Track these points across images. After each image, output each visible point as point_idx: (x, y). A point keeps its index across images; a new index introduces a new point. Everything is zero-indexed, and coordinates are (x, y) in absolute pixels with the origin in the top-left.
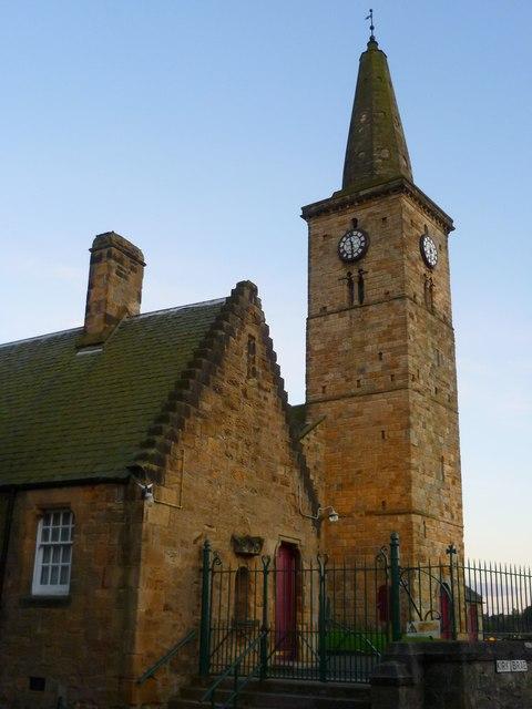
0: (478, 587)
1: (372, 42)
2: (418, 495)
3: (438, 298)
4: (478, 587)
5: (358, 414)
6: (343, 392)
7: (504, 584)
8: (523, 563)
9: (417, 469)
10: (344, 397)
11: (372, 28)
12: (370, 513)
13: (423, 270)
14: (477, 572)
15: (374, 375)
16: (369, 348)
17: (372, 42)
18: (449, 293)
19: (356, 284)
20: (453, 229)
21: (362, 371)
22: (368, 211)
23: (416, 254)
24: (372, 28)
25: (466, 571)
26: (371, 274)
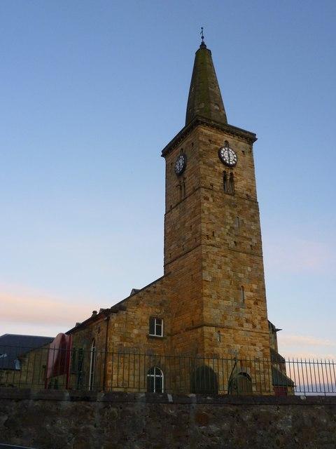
0: (297, 379)
1: (203, 45)
2: (211, 313)
3: (240, 186)
4: (297, 379)
5: (183, 267)
6: (178, 254)
7: (305, 376)
8: (332, 357)
9: (210, 296)
10: (177, 258)
11: (203, 38)
12: (187, 329)
13: (222, 168)
14: (331, 365)
15: (189, 240)
16: (187, 224)
17: (203, 45)
18: (253, 180)
19: (181, 187)
20: (256, 139)
21: (184, 240)
22: (186, 142)
23: (215, 159)
24: (203, 38)
25: (287, 364)
26: (187, 179)
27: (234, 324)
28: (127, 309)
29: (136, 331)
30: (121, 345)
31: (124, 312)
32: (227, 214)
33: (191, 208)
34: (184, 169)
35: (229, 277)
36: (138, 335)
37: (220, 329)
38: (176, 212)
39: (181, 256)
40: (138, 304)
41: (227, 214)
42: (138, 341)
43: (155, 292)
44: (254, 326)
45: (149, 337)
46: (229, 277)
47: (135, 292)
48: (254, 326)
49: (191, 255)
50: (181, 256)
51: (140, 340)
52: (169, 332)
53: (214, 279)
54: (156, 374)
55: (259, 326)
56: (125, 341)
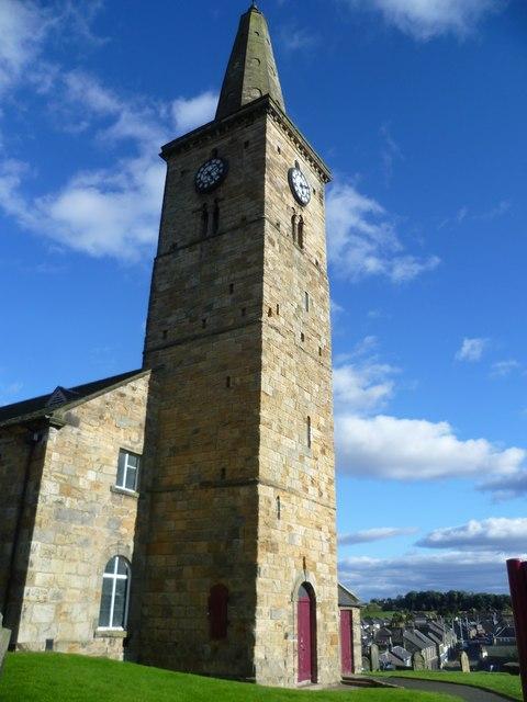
5: (201, 358)
12: (205, 485)
21: (209, 308)
27: (297, 485)
28: (81, 424)
29: (92, 476)
30: (61, 502)
31: (76, 430)
32: (295, 281)
33: (232, 253)
34: (220, 183)
35: (294, 396)
36: (96, 485)
37: (281, 494)
38: (187, 259)
39: (196, 337)
40: (101, 417)
41: (295, 281)
42: (94, 499)
43: (133, 400)
44: (321, 494)
45: (111, 489)
46: (294, 396)
47: (60, 389)
48: (321, 494)
49: (228, 339)
50: (196, 337)
51: (97, 496)
52: (149, 484)
53: (276, 392)
54: (111, 580)
55: (325, 495)
56: (68, 494)
